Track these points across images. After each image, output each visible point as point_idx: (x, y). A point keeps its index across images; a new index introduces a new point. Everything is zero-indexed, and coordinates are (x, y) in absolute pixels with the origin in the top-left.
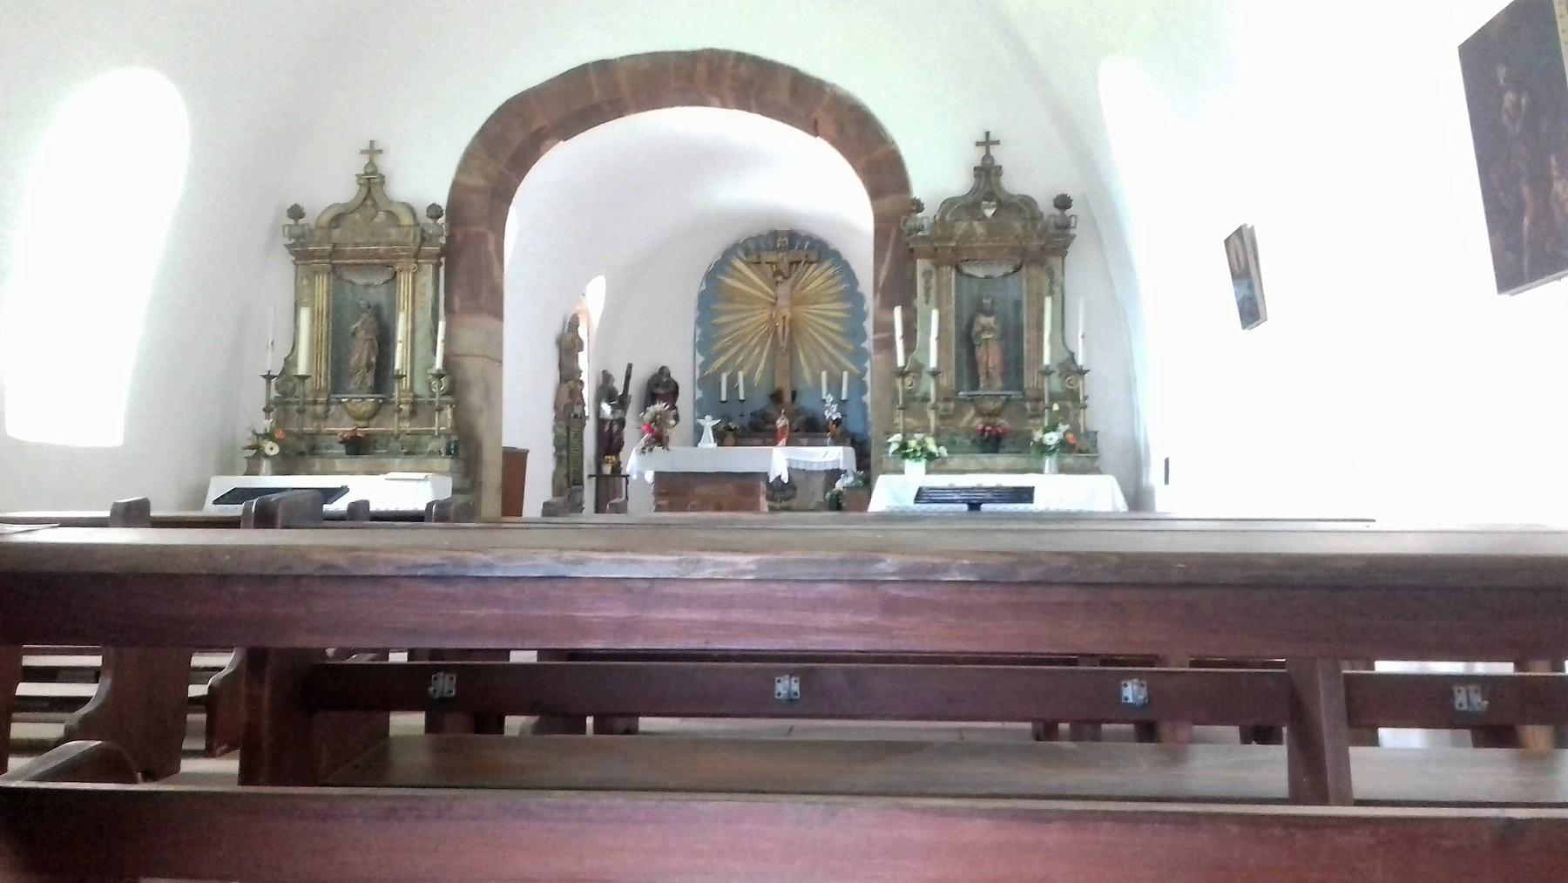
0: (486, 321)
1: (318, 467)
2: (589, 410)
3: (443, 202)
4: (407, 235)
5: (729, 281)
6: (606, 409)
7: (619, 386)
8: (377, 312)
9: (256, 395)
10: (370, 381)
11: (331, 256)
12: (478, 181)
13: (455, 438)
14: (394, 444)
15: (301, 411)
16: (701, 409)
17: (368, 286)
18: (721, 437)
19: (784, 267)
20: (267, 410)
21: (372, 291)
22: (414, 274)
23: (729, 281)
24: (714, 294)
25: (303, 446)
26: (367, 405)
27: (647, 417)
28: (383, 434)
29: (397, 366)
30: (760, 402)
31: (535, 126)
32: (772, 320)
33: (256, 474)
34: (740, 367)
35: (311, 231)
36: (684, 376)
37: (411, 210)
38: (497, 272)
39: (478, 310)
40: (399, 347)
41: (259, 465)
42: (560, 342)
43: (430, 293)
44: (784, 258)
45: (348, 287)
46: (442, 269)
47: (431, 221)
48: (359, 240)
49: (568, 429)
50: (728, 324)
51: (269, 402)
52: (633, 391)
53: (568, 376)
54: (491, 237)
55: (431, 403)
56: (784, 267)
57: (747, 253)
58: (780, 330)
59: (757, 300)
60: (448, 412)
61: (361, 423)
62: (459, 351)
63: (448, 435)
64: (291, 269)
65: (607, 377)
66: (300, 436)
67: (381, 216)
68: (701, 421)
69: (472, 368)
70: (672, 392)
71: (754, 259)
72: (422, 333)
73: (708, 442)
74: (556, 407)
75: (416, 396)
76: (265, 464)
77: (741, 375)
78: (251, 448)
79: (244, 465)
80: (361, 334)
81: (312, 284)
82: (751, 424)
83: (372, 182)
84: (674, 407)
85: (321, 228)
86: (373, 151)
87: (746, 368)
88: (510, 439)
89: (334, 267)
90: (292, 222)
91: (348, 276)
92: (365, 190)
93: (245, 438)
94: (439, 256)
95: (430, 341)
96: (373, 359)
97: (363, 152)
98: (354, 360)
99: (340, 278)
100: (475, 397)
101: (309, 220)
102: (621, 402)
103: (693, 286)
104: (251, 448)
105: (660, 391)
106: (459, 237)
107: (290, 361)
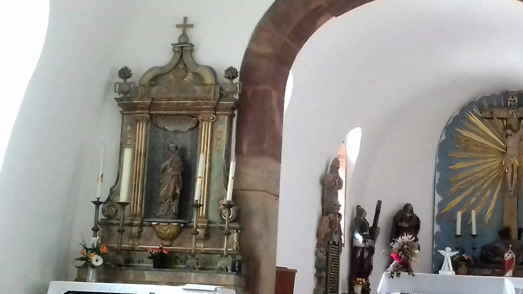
0: (267, 162)
1: (131, 277)
2: (345, 239)
3: (238, 66)
4: (210, 91)
5: (465, 133)
6: (359, 238)
7: (370, 219)
8: (182, 152)
9: (88, 216)
10: (174, 209)
11: (150, 107)
12: (266, 49)
13: (239, 258)
14: (191, 261)
15: (121, 231)
16: (439, 241)
17: (176, 132)
18: (456, 267)
19: (514, 122)
20: (95, 230)
21: (179, 136)
22: (213, 123)
23: (465, 133)
24: (452, 143)
25: (121, 259)
26: (171, 229)
27: (396, 246)
28: (182, 252)
29: (196, 197)
30: (490, 237)
31: (313, 6)
32: (501, 166)
33: (85, 280)
34: (474, 206)
35: (136, 89)
36: (424, 212)
37: (213, 72)
38: (277, 123)
39: (261, 153)
40: (199, 182)
41: (87, 273)
42: (323, 182)
43: (224, 139)
44: (513, 115)
45: (161, 134)
46: (235, 120)
47: (228, 81)
48: (172, 96)
49: (327, 254)
50: (462, 170)
51: (97, 222)
52: (381, 224)
53: (329, 209)
54: (274, 94)
55: (222, 228)
56: (514, 122)
57: (482, 109)
58: (509, 176)
59: (486, 149)
60: (235, 236)
61: (167, 243)
62: (244, 186)
63: (233, 256)
64: (118, 118)
65: (360, 211)
66: (119, 251)
67: (190, 76)
68: (442, 252)
69: (255, 200)
70: (414, 226)
71: (488, 115)
72: (217, 170)
73: (447, 270)
74: (318, 235)
75: (209, 222)
76: (91, 273)
77: (473, 212)
78: (82, 259)
79: (74, 272)
80: (170, 170)
81: (134, 131)
82: (482, 256)
83: (184, 49)
84: (416, 240)
85: (143, 85)
86: (185, 26)
87: (479, 207)
88: (282, 262)
89: (151, 115)
90: (121, 81)
91: (161, 123)
92: (178, 56)
93: (77, 250)
94: (233, 109)
95: (222, 178)
96: (178, 191)
97: (178, 26)
98: (163, 192)
99: (156, 126)
100: (256, 225)
101: (135, 78)
102: (371, 233)
103: (434, 136)
104: (82, 259)
105: (405, 225)
106: (249, 94)
107: (114, 191)
